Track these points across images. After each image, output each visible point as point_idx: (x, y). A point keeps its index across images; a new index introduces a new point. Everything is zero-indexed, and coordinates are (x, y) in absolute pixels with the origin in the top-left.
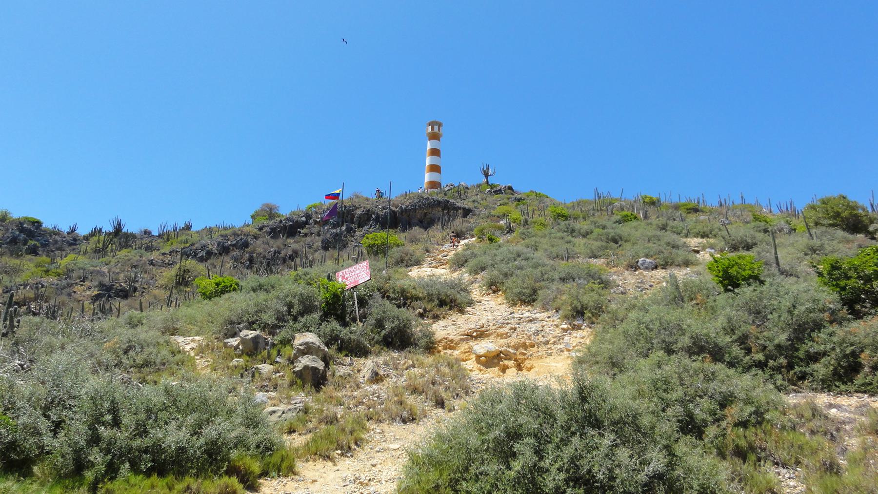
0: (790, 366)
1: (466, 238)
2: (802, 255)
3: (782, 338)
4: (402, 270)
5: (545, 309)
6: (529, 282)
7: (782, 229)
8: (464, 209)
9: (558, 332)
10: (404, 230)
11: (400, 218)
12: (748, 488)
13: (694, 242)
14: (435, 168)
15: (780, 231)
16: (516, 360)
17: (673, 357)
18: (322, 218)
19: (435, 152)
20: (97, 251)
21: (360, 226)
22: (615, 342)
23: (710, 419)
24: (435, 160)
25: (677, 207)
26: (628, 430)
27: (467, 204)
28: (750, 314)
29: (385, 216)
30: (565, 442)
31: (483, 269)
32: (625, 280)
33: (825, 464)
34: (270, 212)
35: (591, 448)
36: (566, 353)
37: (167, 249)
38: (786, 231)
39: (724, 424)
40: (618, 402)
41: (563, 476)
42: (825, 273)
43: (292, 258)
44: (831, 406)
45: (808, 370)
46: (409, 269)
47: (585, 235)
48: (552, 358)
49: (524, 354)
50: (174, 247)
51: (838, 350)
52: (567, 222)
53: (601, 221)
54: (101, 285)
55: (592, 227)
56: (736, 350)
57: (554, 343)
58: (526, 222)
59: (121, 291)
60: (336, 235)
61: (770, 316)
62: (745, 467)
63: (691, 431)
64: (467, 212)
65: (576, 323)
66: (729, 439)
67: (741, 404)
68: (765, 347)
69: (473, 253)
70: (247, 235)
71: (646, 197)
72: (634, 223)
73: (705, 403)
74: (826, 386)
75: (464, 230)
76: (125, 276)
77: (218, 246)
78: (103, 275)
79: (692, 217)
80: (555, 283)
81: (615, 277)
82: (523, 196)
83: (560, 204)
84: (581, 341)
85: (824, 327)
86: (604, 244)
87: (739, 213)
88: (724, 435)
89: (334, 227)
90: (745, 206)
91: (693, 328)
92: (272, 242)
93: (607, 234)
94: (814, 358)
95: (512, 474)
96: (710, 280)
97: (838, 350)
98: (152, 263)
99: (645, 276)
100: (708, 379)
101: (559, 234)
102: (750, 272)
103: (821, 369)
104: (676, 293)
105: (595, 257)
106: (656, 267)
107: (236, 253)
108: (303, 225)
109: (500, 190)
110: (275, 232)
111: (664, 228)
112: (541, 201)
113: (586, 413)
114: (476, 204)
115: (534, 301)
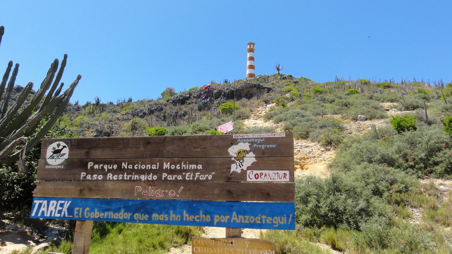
0: (426, 167)
1: (270, 104)
2: (441, 112)
3: (423, 155)
4: (240, 121)
5: (313, 141)
6: (305, 128)
7: (434, 97)
8: (268, 88)
9: (319, 152)
10: (238, 99)
11: (235, 94)
12: (399, 215)
13: (387, 105)
14: (251, 67)
15: (433, 98)
16: (300, 165)
17: (371, 164)
18: (197, 95)
19: (251, 59)
20: (90, 113)
21: (216, 98)
22: (346, 157)
23: (386, 189)
24: (251, 63)
25: (378, 86)
26: (352, 193)
27: (269, 85)
28: (408, 144)
29: (228, 93)
30: (327, 197)
31: (281, 121)
32: (351, 126)
33: (431, 207)
34: (171, 92)
35: (337, 200)
36: (323, 162)
37: (124, 112)
38: (436, 97)
39: (391, 191)
40: (347, 183)
41: (327, 209)
42: (447, 124)
43: (184, 115)
44: (441, 184)
45: (434, 169)
46: (243, 120)
47: (332, 102)
48: (317, 164)
49: (304, 162)
50: (127, 111)
51: (447, 160)
52: (321, 95)
53: (339, 95)
54: (97, 130)
55: (334, 97)
56: (401, 161)
57: (318, 157)
58: (300, 95)
59: (106, 133)
60: (205, 103)
61: (417, 145)
62: (398, 208)
63: (378, 195)
64: (269, 90)
65: (328, 148)
66: (393, 197)
67: (399, 184)
68: (415, 159)
69: (275, 113)
70: (161, 104)
71: (362, 80)
72: (356, 95)
73: (384, 183)
74: (441, 176)
75: (269, 100)
76: (107, 126)
77: (148, 110)
78: (97, 126)
79: (387, 90)
80: (317, 129)
81: (346, 125)
82: (297, 80)
83: (317, 84)
84: (331, 156)
85: (442, 150)
86: (340, 107)
87: (412, 87)
88: (391, 196)
89: (204, 99)
90: (416, 83)
91: (382, 151)
92: (173, 107)
93: (342, 102)
94: (436, 164)
95: (308, 208)
96: (392, 128)
97: (447, 160)
98: (118, 119)
99: (361, 124)
100: (387, 173)
101: (318, 102)
102: (410, 124)
103: (439, 169)
104: (375, 134)
105: (336, 114)
106: (366, 119)
107: (157, 113)
108: (188, 98)
109: (286, 77)
110: (175, 103)
111: (371, 98)
112: (307, 83)
113: (335, 187)
114: (274, 86)
115: (307, 137)
